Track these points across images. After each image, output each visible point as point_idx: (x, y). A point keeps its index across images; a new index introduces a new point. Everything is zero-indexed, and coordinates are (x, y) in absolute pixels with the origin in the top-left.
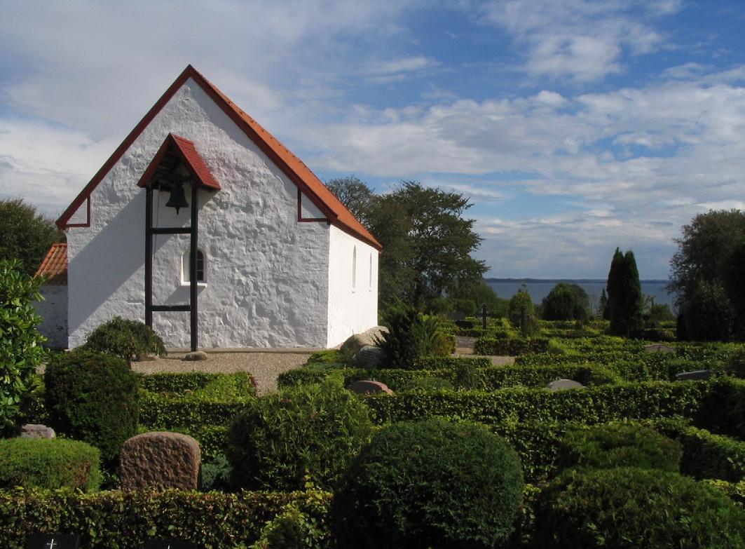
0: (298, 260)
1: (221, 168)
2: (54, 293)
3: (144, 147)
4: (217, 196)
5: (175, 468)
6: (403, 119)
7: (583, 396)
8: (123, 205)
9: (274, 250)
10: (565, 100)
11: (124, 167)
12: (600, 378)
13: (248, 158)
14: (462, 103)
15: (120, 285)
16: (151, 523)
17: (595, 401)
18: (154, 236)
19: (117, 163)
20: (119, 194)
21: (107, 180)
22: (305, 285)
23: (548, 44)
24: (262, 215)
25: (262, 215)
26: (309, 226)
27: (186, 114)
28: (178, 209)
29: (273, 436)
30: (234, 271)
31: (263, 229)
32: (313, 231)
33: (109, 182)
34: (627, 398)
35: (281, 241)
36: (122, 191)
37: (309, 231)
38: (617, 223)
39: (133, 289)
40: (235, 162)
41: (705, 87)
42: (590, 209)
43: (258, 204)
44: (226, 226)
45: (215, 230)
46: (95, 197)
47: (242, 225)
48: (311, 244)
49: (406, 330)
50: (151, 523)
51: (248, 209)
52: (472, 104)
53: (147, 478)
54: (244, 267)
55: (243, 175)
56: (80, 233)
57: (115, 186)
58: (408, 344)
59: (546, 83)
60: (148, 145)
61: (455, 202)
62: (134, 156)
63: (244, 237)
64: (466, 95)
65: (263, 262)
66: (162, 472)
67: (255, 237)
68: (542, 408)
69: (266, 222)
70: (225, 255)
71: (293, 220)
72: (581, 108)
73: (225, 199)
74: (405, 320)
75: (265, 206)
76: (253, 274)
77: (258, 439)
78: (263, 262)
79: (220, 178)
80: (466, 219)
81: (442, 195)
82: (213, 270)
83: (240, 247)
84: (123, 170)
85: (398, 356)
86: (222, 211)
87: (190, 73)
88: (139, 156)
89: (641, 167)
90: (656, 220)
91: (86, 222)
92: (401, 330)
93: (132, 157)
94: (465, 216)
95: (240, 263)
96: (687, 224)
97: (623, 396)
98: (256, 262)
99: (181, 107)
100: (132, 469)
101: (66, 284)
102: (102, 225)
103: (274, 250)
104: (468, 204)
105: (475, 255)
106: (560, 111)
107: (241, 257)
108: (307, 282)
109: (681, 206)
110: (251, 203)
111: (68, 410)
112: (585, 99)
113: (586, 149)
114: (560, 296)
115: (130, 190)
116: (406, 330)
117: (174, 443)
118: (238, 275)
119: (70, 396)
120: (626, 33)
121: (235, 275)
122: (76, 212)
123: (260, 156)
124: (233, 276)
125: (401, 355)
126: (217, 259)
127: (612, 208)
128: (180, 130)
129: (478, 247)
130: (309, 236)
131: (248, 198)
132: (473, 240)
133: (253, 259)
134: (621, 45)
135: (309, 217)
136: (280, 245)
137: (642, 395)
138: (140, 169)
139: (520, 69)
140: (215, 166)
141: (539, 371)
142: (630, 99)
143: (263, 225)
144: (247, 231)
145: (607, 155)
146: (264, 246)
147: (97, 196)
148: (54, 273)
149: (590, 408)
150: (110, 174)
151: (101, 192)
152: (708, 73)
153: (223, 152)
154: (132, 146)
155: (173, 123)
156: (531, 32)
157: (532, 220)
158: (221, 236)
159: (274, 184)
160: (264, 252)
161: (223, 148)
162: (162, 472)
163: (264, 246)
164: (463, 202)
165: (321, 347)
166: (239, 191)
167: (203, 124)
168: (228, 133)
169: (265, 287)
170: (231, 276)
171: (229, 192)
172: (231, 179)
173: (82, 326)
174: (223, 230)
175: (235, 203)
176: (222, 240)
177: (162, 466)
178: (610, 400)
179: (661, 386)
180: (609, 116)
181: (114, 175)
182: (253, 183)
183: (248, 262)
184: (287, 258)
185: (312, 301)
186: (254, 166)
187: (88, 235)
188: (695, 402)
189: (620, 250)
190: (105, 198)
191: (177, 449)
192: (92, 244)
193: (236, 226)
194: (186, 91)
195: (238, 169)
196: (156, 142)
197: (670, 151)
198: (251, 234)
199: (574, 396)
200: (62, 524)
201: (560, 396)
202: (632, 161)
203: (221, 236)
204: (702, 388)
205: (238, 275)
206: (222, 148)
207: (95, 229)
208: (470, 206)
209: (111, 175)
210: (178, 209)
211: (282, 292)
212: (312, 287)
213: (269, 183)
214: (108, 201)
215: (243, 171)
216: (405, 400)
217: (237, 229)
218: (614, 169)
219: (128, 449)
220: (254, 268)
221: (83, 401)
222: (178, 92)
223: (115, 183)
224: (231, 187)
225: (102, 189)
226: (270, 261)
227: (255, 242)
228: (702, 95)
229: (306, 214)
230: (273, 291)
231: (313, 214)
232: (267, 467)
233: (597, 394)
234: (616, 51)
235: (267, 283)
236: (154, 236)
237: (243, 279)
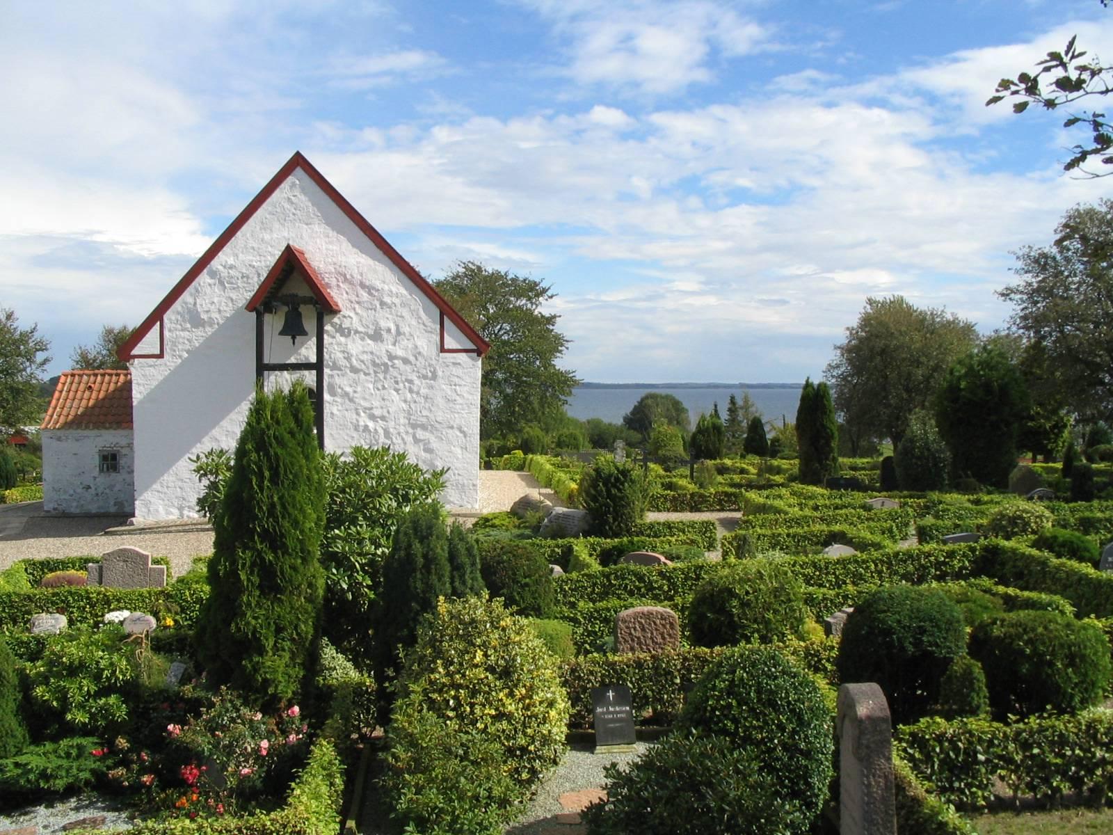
0: (440, 401)
1: (341, 284)
2: (77, 440)
3: (237, 256)
4: (336, 320)
5: (662, 634)
6: (391, 145)
7: (864, 562)
8: (209, 330)
9: (410, 388)
10: (631, 120)
11: (211, 281)
12: (859, 542)
13: (375, 271)
14: (478, 122)
15: (207, 433)
16: (676, 673)
17: (876, 565)
18: (266, 373)
19: (201, 276)
20: (204, 316)
21: (186, 296)
22: (450, 431)
23: (602, 37)
24: (394, 344)
25: (394, 344)
26: (454, 358)
27: (294, 214)
28: (294, 338)
29: (744, 605)
30: (358, 414)
31: (396, 361)
32: (459, 364)
33: (191, 300)
34: (905, 562)
35: (419, 377)
36: (208, 312)
37: (454, 364)
38: (712, 300)
39: (224, 438)
40: (359, 277)
41: (829, 105)
42: (673, 281)
43: (389, 331)
44: (348, 359)
45: (334, 363)
46: (170, 319)
47: (370, 357)
48: (456, 380)
49: (620, 490)
50: (676, 673)
51: (377, 336)
52: (493, 123)
53: (640, 643)
54: (371, 409)
55: (370, 294)
56: (151, 366)
57: (198, 306)
58: (623, 506)
59: (603, 94)
60: (242, 252)
61: (532, 290)
62: (225, 267)
63: (372, 372)
64: (484, 111)
65: (396, 403)
66: (651, 638)
67: (386, 371)
68: (827, 574)
69: (400, 353)
70: (347, 394)
71: (434, 350)
72: (653, 131)
73: (346, 324)
74: (617, 479)
75: (399, 333)
76: (383, 418)
77: (734, 607)
78: (396, 403)
79: (338, 295)
80: (546, 313)
81: (514, 280)
82: (332, 413)
83: (366, 385)
84: (210, 285)
85: (611, 520)
86: (343, 339)
87: (298, 162)
88: (231, 267)
89: (741, 219)
90: (765, 297)
91: (157, 352)
92: (614, 491)
93: (220, 268)
94: (544, 308)
95: (367, 405)
96: (850, 326)
97: (901, 560)
98: (387, 402)
99: (287, 206)
100: (628, 638)
101: (132, 428)
102: (180, 357)
103: (410, 388)
104: (549, 293)
105: (562, 363)
106: (624, 136)
107: (367, 397)
108: (452, 427)
109: (799, 276)
110: (380, 329)
111: (515, 594)
112: (659, 119)
113: (661, 192)
114: (708, 428)
115: (220, 311)
116: (620, 490)
117: (662, 615)
118: (364, 420)
119: (515, 582)
120: (714, 25)
121: (360, 419)
122: (144, 339)
123: (391, 270)
124: (357, 421)
125: (615, 520)
126: (336, 399)
127: (703, 278)
128: (286, 235)
129: (565, 351)
130: (455, 370)
131: (376, 323)
132: (556, 344)
133: (383, 399)
134: (708, 41)
135: (454, 348)
136: (417, 382)
137: (919, 559)
138: (232, 283)
139: (565, 72)
140: (333, 282)
141: (788, 535)
142: (723, 121)
143: (396, 357)
144: (374, 364)
145: (694, 201)
146: (397, 383)
147: (173, 318)
148: (73, 413)
149: (872, 572)
150: (191, 289)
151: (178, 313)
152: (833, 85)
153: (343, 264)
154: (220, 254)
155: (276, 225)
156: (574, 18)
157: (588, 297)
158: (341, 370)
159: (409, 306)
160: (397, 390)
161: (343, 259)
162: (651, 638)
163: (397, 383)
164: (544, 291)
165: (469, 506)
166: (365, 314)
167: (316, 228)
168: (349, 240)
169: (399, 434)
170: (354, 421)
171: (352, 314)
172: (354, 298)
173: (154, 486)
174: (343, 362)
175: (361, 329)
176: (343, 375)
177: (652, 633)
178: (890, 565)
179: (935, 549)
180: (694, 144)
181: (197, 291)
182: (382, 304)
183: (376, 403)
184: (426, 398)
185: (459, 451)
186: (384, 282)
187: (162, 368)
188: (967, 563)
189: (810, 381)
190: (184, 321)
191: (665, 619)
192: (166, 380)
193: (362, 358)
194: (293, 185)
195: (363, 286)
196: (253, 248)
197: (781, 197)
198: (382, 367)
199: (856, 561)
200: (603, 680)
201: (842, 562)
202: (729, 211)
203: (341, 370)
204: (973, 550)
205: (364, 420)
206: (342, 259)
207: (170, 361)
208: (551, 297)
209: (193, 291)
210: (294, 338)
211: (421, 441)
212: (458, 433)
213: (403, 305)
214: (188, 326)
215: (370, 289)
216: (695, 571)
217: (362, 361)
218: (703, 221)
219: (624, 621)
220: (385, 410)
221: (527, 585)
222: (282, 185)
223: (198, 301)
224: (354, 309)
225: (180, 309)
226: (405, 401)
227: (385, 378)
228: (823, 118)
229: (450, 343)
230: (409, 439)
231: (459, 342)
232: (744, 627)
233: (877, 559)
234: (701, 50)
235: (402, 429)
236: (266, 373)
237: (371, 425)
